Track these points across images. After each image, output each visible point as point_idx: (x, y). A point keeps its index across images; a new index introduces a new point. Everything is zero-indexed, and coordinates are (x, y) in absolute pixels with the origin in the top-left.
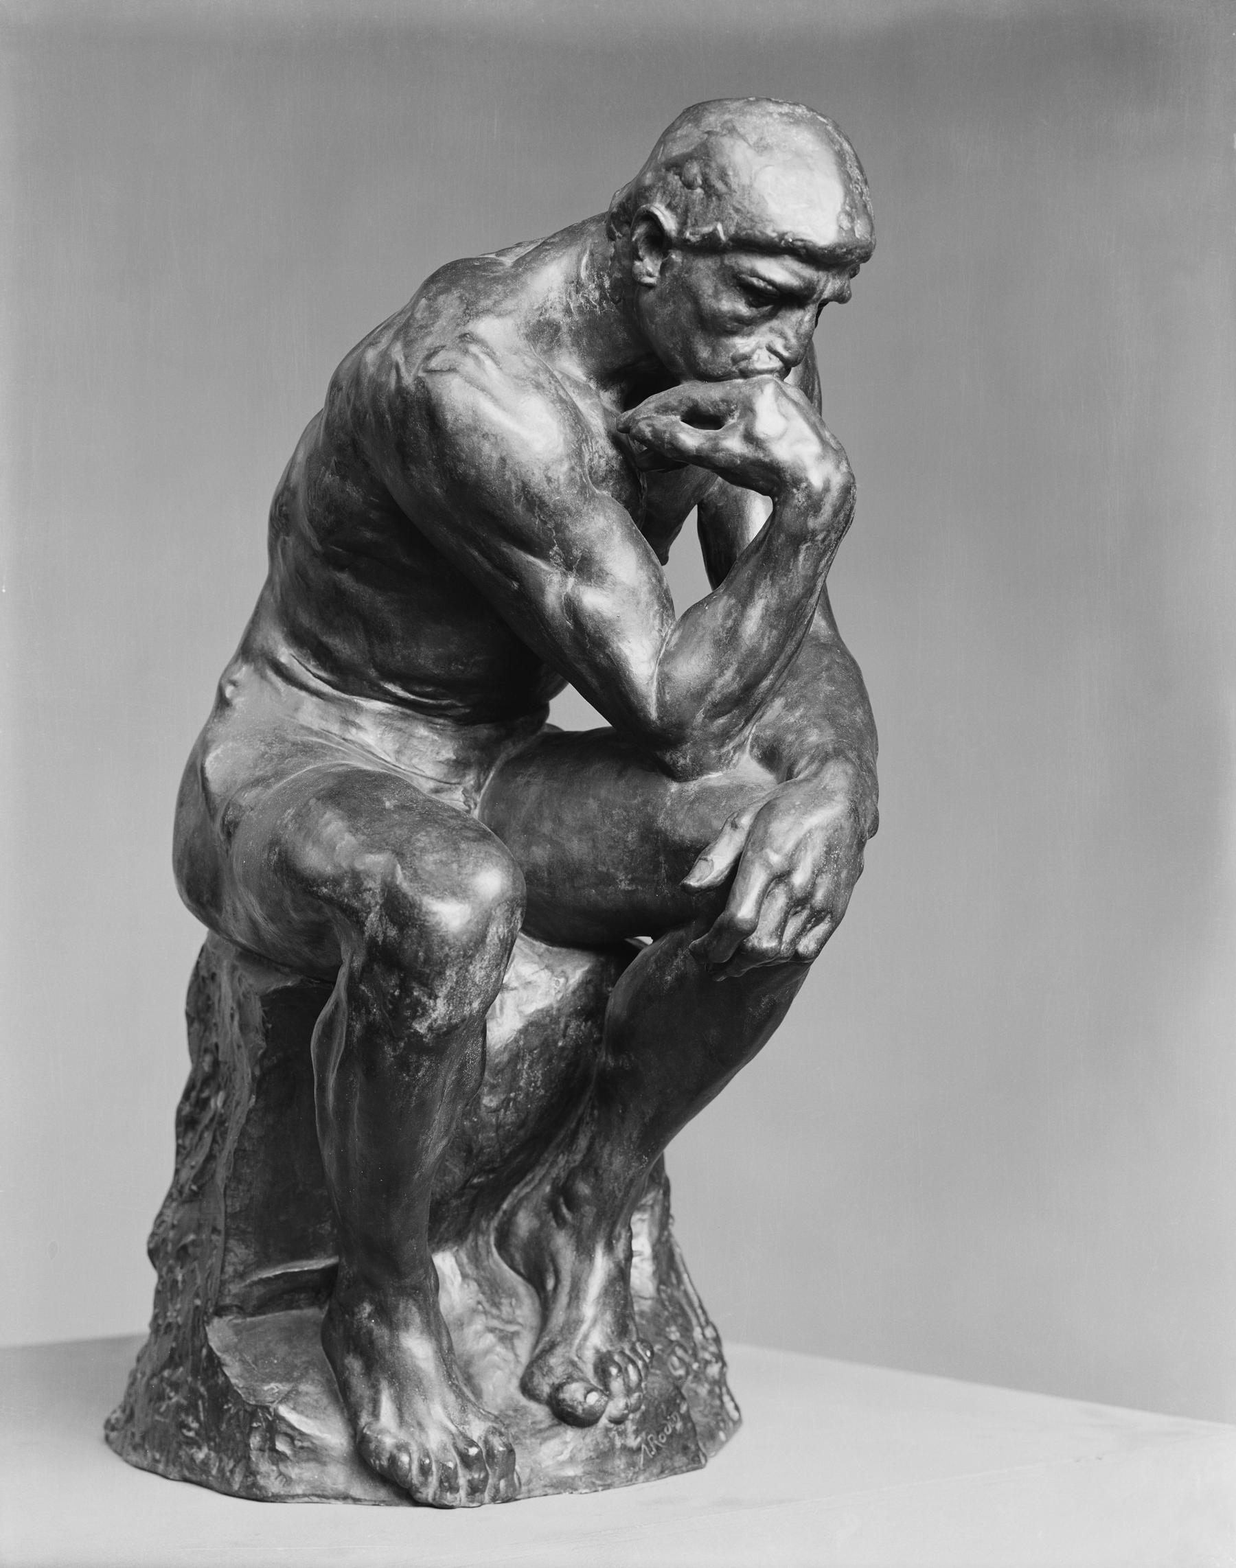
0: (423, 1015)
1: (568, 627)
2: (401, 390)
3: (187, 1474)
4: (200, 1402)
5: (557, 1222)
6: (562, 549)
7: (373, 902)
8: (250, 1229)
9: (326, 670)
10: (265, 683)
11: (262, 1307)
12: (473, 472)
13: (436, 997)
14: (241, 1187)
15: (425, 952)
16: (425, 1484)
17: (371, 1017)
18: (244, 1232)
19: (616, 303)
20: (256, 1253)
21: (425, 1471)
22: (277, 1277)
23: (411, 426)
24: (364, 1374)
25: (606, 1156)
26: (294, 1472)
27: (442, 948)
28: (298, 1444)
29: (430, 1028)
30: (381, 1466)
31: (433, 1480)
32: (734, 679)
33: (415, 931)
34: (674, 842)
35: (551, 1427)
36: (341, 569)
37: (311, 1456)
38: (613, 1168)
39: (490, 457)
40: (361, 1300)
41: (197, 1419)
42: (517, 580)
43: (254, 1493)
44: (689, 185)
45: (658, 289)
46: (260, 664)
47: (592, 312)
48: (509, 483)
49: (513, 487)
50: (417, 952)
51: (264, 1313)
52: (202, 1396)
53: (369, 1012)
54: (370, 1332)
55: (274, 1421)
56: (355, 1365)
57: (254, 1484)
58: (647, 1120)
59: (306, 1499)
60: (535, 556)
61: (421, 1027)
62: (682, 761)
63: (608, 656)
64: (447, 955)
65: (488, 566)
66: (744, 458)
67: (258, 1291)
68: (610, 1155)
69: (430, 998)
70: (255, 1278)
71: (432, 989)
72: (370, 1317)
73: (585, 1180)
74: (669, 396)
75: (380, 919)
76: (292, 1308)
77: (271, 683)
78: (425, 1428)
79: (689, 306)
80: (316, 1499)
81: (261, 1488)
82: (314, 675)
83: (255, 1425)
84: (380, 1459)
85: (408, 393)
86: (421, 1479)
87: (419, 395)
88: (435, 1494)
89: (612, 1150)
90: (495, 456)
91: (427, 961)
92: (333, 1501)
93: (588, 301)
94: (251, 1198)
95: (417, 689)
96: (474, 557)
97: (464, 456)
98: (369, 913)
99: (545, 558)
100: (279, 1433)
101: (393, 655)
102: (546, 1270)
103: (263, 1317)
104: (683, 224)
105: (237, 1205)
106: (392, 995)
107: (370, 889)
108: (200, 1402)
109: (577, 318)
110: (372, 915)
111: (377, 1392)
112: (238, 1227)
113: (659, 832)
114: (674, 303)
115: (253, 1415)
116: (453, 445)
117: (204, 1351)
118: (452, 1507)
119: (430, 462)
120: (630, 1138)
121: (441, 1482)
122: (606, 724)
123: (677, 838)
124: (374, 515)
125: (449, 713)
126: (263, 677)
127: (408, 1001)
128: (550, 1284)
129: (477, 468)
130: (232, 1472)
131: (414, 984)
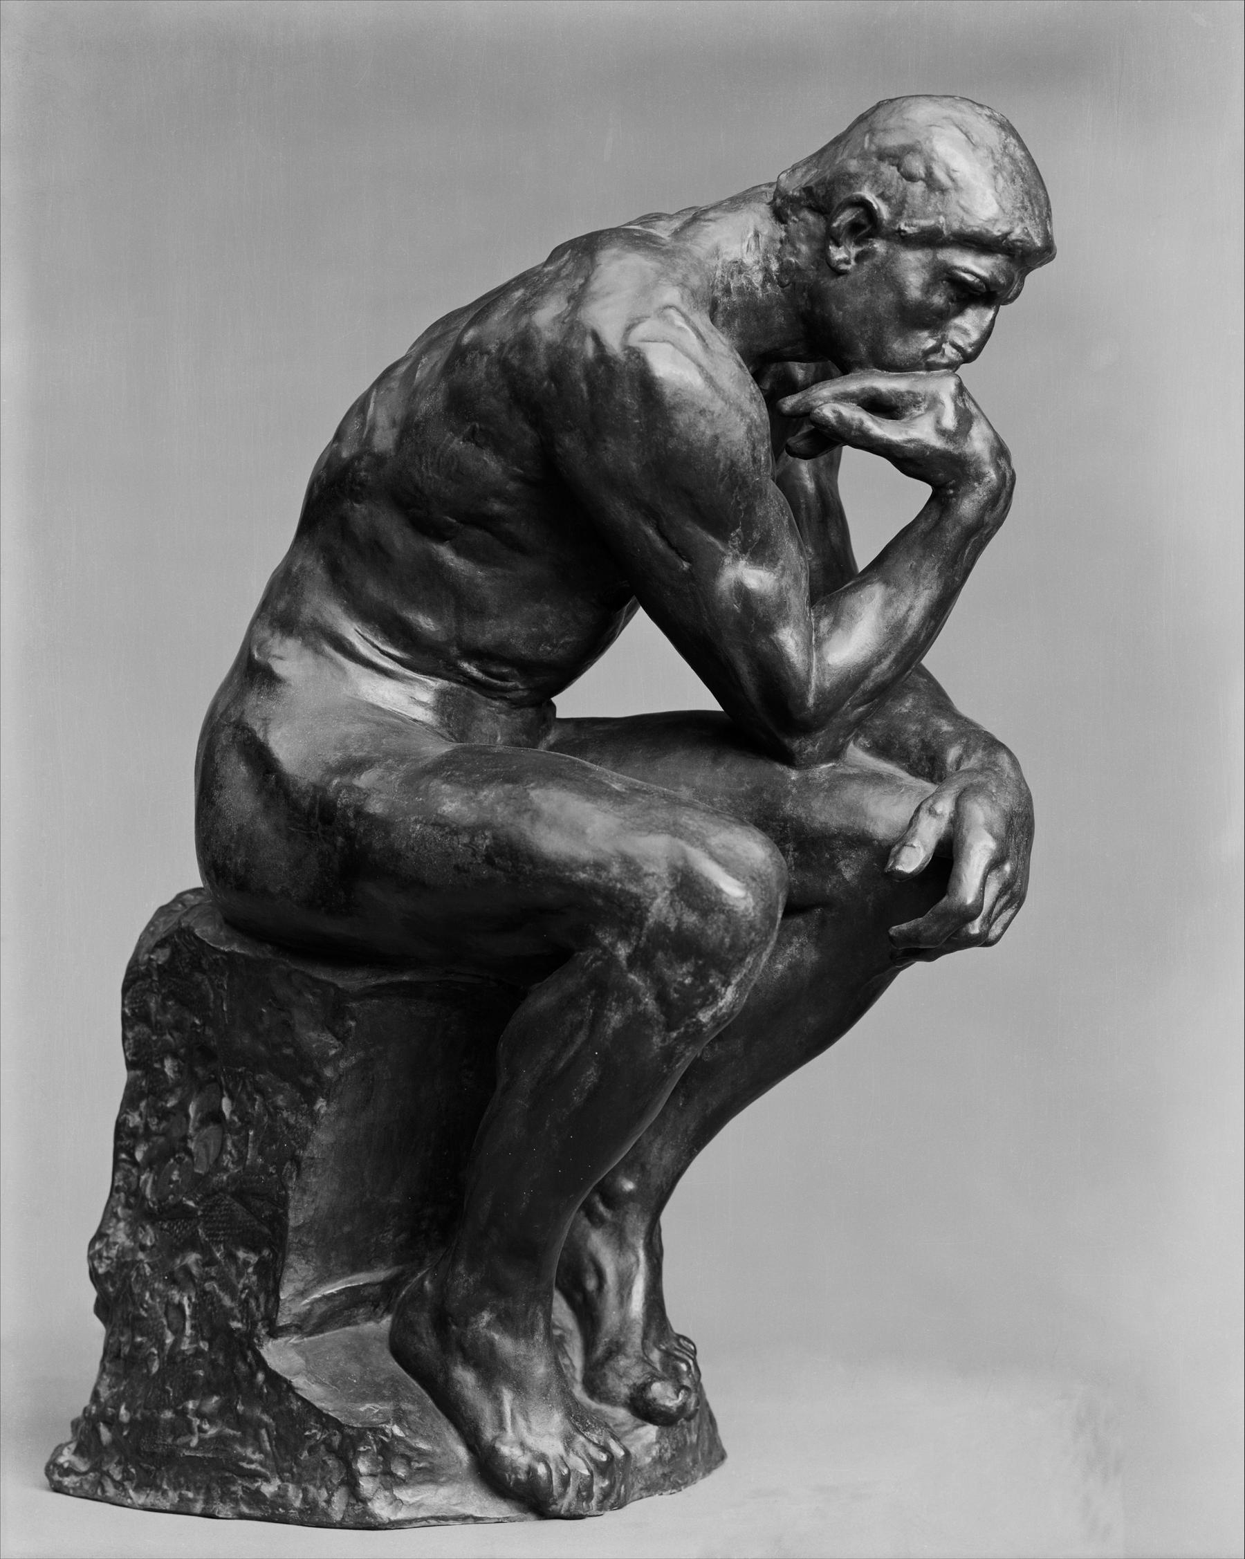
0: (712, 1003)
1: (734, 610)
2: (603, 356)
3: (245, 1509)
4: (263, 1432)
5: (591, 1220)
6: (744, 531)
7: (659, 888)
8: (312, 1243)
9: (396, 647)
10: (321, 660)
11: (319, 1328)
12: (684, 448)
13: (730, 984)
14: (305, 1198)
15: (732, 938)
16: (563, 1495)
17: (641, 1007)
18: (306, 1246)
19: (782, 286)
20: (316, 1269)
21: (565, 1482)
22: (341, 1292)
23: (617, 397)
24: (482, 1386)
25: (655, 1151)
26: (404, 1494)
27: (749, 934)
28: (416, 1465)
29: (713, 1017)
30: (517, 1480)
31: (571, 1491)
32: (890, 668)
33: (722, 917)
34: (814, 830)
35: (638, 1427)
36: (441, 538)
37: (428, 1478)
38: (663, 1162)
39: (704, 433)
40: (481, 1309)
41: (261, 1450)
42: (689, 561)
43: (366, 1523)
44: (911, 178)
45: (851, 277)
46: (312, 639)
47: (752, 294)
48: (718, 461)
49: (721, 466)
50: (723, 938)
51: (322, 1332)
52: (266, 1426)
53: (638, 1002)
54: (491, 1343)
55: (391, 1443)
56: (466, 1378)
57: (366, 1512)
58: (708, 1112)
59: (424, 1523)
60: (716, 536)
61: (704, 1017)
62: (810, 749)
63: (772, 642)
64: (752, 941)
65: (660, 545)
66: (935, 450)
67: (321, 1309)
68: (661, 1149)
69: (723, 986)
70: (317, 1296)
71: (728, 977)
72: (489, 1325)
73: (629, 1178)
74: (853, 385)
75: (671, 904)
76: (349, 1325)
77: (331, 659)
78: (534, 1436)
79: (891, 296)
80: (433, 1522)
81: (373, 1516)
82: (383, 652)
83: (362, 1449)
84: (516, 1473)
85: (616, 362)
86: (560, 1490)
87: (631, 365)
88: (570, 1504)
89: (663, 1145)
90: (709, 432)
91: (732, 947)
92: (451, 1522)
93: (750, 282)
94: (316, 1209)
95: (494, 670)
96: (647, 537)
97: (677, 431)
98: (654, 899)
99: (725, 539)
100: (396, 1455)
101: (484, 634)
102: (585, 1271)
103: (321, 1336)
104: (897, 214)
105: (301, 1217)
106: (682, 984)
107: (653, 874)
108: (263, 1432)
109: (735, 298)
110: (659, 901)
111: (497, 1399)
112: (300, 1241)
113: (786, 820)
114: (872, 292)
115: (360, 1437)
116: (667, 419)
117: (260, 1377)
118: (581, 1517)
119: (634, 436)
120: (686, 1131)
121: (579, 1492)
122: (721, 709)
123: (817, 825)
124: (512, 486)
125: (508, 696)
126: (318, 652)
127: (702, 989)
128: (591, 1284)
129: (688, 442)
130: (329, 1502)
131: (713, 972)
